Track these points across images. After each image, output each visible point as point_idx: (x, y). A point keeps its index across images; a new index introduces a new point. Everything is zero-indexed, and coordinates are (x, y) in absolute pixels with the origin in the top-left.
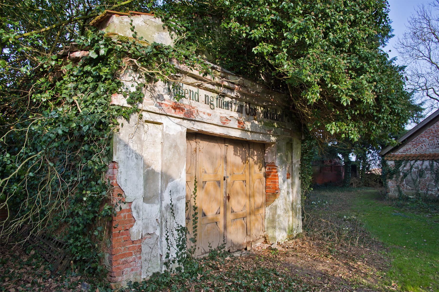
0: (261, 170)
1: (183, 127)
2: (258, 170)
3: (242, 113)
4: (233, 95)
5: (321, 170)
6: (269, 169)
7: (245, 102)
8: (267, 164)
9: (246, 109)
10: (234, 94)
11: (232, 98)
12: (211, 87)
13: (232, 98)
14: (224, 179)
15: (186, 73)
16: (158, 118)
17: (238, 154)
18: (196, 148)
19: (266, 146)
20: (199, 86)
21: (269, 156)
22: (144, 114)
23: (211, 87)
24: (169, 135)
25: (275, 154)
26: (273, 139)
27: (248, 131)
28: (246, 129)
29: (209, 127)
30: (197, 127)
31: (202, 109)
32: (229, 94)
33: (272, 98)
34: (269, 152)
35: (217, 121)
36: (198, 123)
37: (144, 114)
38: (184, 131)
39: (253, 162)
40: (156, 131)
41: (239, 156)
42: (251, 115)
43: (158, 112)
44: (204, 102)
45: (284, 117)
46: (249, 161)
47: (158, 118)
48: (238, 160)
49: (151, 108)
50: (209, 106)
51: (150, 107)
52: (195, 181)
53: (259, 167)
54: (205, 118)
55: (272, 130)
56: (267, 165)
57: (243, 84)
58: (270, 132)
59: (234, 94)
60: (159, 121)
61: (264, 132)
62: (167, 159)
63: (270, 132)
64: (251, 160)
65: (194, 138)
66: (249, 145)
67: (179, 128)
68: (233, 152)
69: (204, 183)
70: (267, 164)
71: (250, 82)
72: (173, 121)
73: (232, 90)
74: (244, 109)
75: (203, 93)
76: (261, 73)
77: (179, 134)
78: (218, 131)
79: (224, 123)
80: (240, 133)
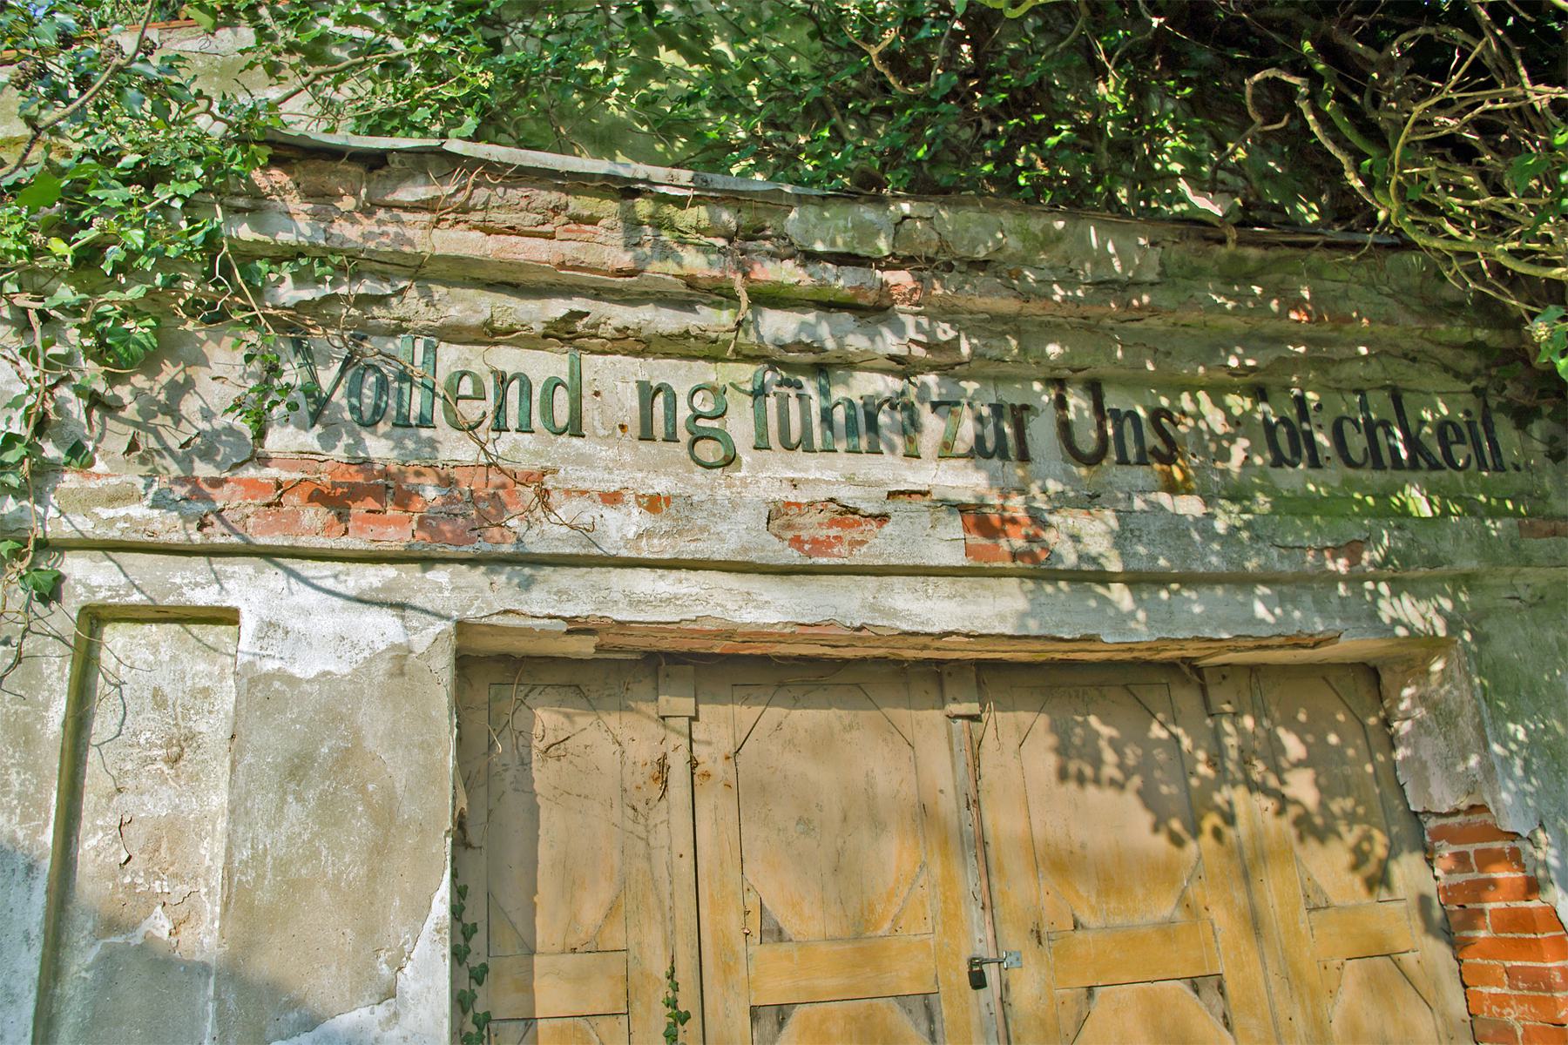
0: (1379, 880)
1: (415, 619)
2: (1357, 881)
3: (1024, 457)
4: (890, 343)
5: (392, 606)
6: (1461, 859)
7: (1050, 382)
8: (1432, 823)
9: (1065, 428)
10: (899, 330)
11: (902, 366)
12: (667, 320)
13: (902, 366)
14: (978, 981)
15: (423, 271)
16: (194, 585)
17: (1110, 770)
18: (663, 765)
19: (1386, 678)
20: (563, 333)
21: (1426, 755)
22: (74, 566)
23: (667, 320)
24: (291, 681)
25: (1469, 733)
26: (1411, 612)
27: (1105, 578)
28: (1070, 559)
29: (683, 589)
30: (546, 605)
31: (602, 482)
32: (857, 342)
33: (1298, 304)
34: (1419, 724)
35: (734, 535)
36: (565, 578)
37: (74, 566)
38: (430, 639)
39: (1285, 823)
40: (202, 666)
41: (1119, 786)
42: (1123, 461)
43: (176, 538)
44: (635, 429)
45: (1506, 431)
46: (1230, 819)
47: (194, 585)
48: (1119, 820)
49: (111, 521)
50: (681, 449)
51: (106, 513)
52: (672, 1003)
53: (1360, 857)
54: (621, 528)
55: (1372, 540)
56: (1439, 834)
57: (943, 246)
58: (1354, 560)
59: (899, 330)
60: (204, 597)
61: (1286, 567)
62: (257, 858)
63: (1354, 560)
64: (1252, 809)
65: (644, 688)
66: (1203, 689)
67: (382, 628)
68: (1042, 760)
69: (768, 1024)
70: (1432, 823)
71: (1007, 219)
72: (329, 584)
73: (873, 311)
74: (1042, 431)
75: (616, 380)
76: (1184, 175)
77: (383, 667)
78: (767, 609)
79: (819, 545)
80: (1021, 604)
